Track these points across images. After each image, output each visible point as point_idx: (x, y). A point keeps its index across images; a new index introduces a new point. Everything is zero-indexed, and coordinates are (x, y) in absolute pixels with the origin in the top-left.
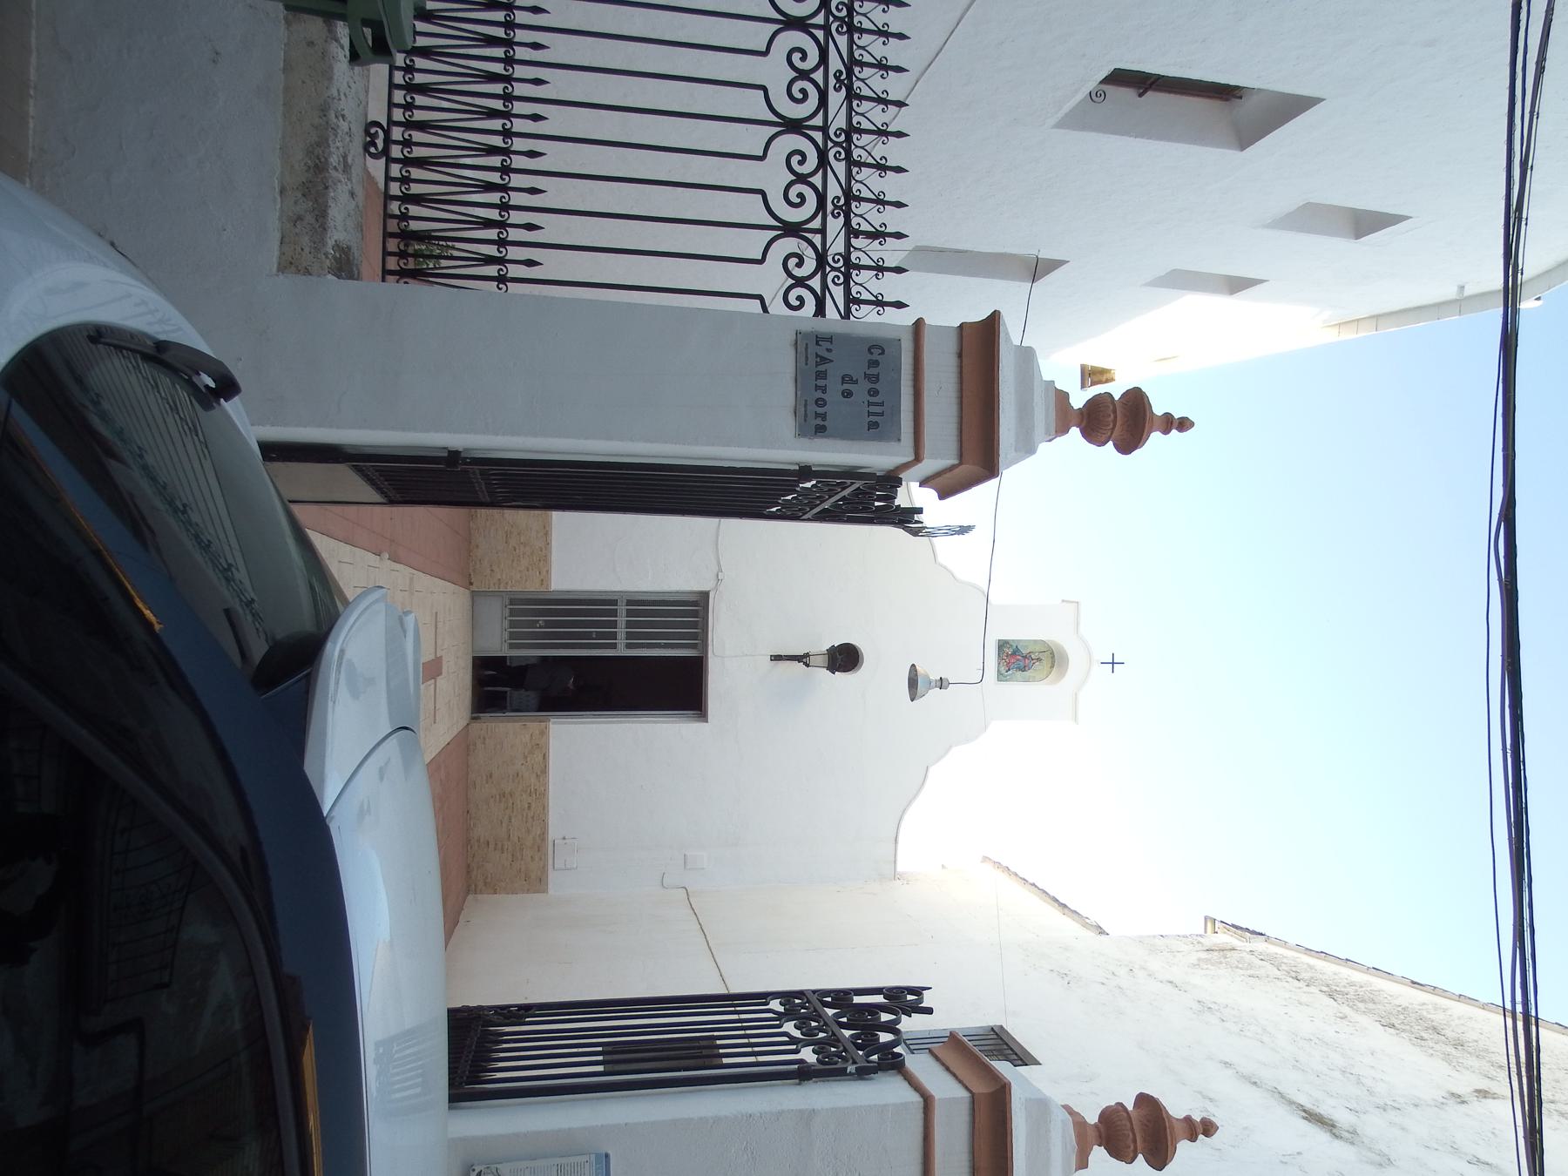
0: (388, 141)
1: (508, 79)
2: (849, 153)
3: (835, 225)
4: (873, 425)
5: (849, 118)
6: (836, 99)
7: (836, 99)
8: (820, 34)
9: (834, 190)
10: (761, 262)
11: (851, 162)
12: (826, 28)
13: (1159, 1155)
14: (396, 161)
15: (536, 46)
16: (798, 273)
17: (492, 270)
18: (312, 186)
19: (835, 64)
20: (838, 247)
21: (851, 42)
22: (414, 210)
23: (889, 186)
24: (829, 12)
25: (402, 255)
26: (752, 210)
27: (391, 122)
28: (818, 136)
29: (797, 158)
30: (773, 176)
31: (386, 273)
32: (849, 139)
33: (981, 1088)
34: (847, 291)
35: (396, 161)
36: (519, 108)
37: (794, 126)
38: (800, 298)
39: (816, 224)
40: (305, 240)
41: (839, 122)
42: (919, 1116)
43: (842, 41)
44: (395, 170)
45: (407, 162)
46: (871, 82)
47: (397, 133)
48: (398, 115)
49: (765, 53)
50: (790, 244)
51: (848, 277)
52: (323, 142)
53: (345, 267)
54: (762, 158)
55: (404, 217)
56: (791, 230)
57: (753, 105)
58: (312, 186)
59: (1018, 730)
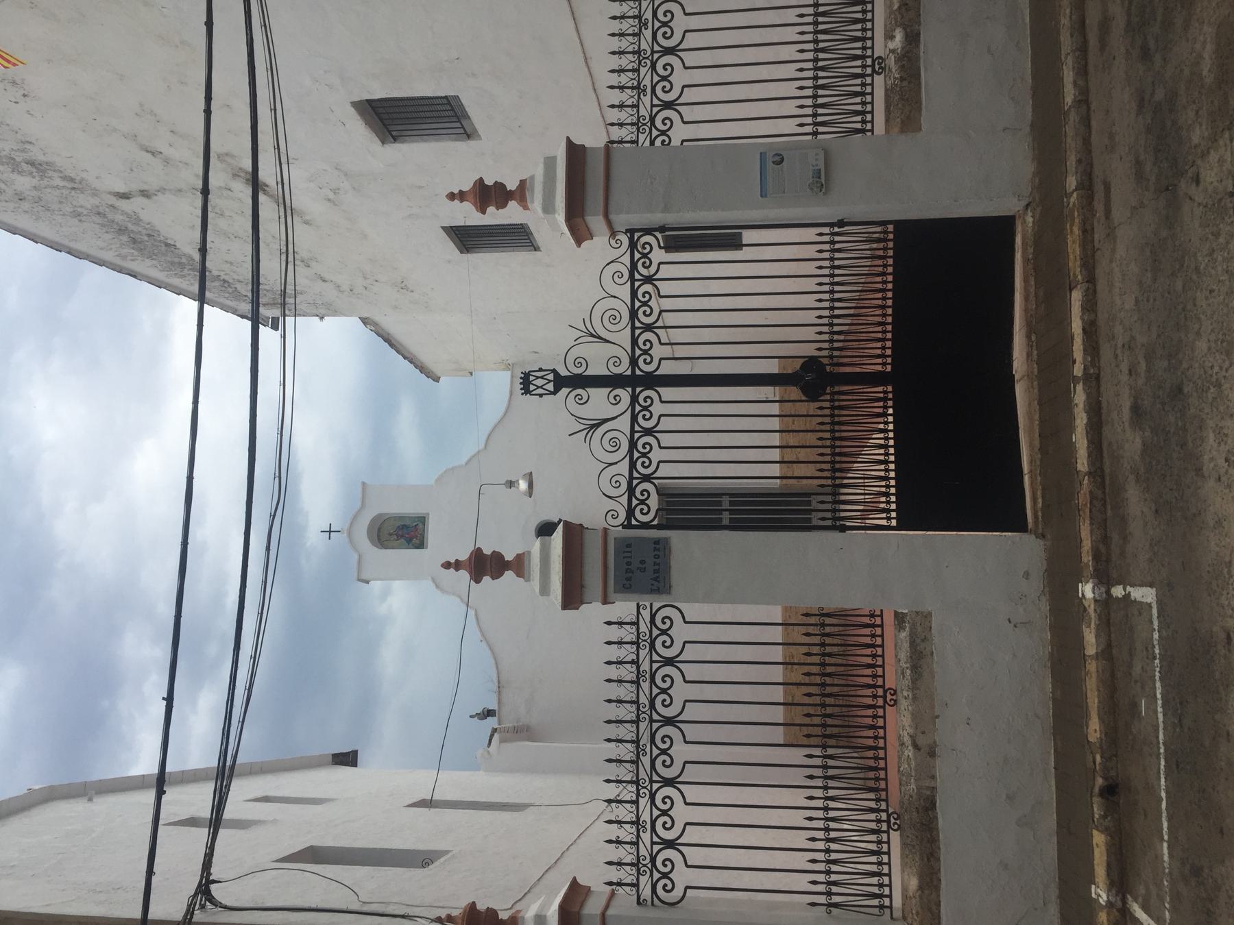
0: (888, 821)
1: (815, 124)
2: (638, 709)
3: (645, 666)
4: (629, 546)
5: (638, 808)
6: (645, 740)
7: (645, 740)
8: (655, 778)
9: (645, 686)
10: (685, 642)
11: (636, 702)
12: (651, 781)
13: (478, 554)
14: (883, 811)
15: (802, 107)
16: (666, 819)
17: (821, 9)
18: (919, 658)
19: (646, 760)
20: (643, 653)
21: (637, 776)
22: (873, 805)
23: (615, 653)
24: (650, 792)
25: (877, 779)
26: (692, 731)
27: (883, 707)
28: (655, 717)
29: (668, 644)
30: (680, 691)
31: (881, 616)
32: (638, 716)
33: (579, 220)
34: (638, 629)
35: (883, 811)
36: (821, 824)
37: (669, 721)
38: (665, 866)
39: (655, 666)
40: (919, 629)
41: (643, 726)
42: (611, 209)
43: (642, 774)
44: (869, 52)
45: (874, 686)
46: (626, 751)
47: (880, 702)
48: (869, 80)
49: (684, 87)
50: (668, 712)
51: (638, 637)
52: (914, 681)
53: (900, 618)
54: (687, 824)
55: (878, 800)
56: (669, 662)
57: (692, 671)
58: (919, 658)
59: (554, 347)
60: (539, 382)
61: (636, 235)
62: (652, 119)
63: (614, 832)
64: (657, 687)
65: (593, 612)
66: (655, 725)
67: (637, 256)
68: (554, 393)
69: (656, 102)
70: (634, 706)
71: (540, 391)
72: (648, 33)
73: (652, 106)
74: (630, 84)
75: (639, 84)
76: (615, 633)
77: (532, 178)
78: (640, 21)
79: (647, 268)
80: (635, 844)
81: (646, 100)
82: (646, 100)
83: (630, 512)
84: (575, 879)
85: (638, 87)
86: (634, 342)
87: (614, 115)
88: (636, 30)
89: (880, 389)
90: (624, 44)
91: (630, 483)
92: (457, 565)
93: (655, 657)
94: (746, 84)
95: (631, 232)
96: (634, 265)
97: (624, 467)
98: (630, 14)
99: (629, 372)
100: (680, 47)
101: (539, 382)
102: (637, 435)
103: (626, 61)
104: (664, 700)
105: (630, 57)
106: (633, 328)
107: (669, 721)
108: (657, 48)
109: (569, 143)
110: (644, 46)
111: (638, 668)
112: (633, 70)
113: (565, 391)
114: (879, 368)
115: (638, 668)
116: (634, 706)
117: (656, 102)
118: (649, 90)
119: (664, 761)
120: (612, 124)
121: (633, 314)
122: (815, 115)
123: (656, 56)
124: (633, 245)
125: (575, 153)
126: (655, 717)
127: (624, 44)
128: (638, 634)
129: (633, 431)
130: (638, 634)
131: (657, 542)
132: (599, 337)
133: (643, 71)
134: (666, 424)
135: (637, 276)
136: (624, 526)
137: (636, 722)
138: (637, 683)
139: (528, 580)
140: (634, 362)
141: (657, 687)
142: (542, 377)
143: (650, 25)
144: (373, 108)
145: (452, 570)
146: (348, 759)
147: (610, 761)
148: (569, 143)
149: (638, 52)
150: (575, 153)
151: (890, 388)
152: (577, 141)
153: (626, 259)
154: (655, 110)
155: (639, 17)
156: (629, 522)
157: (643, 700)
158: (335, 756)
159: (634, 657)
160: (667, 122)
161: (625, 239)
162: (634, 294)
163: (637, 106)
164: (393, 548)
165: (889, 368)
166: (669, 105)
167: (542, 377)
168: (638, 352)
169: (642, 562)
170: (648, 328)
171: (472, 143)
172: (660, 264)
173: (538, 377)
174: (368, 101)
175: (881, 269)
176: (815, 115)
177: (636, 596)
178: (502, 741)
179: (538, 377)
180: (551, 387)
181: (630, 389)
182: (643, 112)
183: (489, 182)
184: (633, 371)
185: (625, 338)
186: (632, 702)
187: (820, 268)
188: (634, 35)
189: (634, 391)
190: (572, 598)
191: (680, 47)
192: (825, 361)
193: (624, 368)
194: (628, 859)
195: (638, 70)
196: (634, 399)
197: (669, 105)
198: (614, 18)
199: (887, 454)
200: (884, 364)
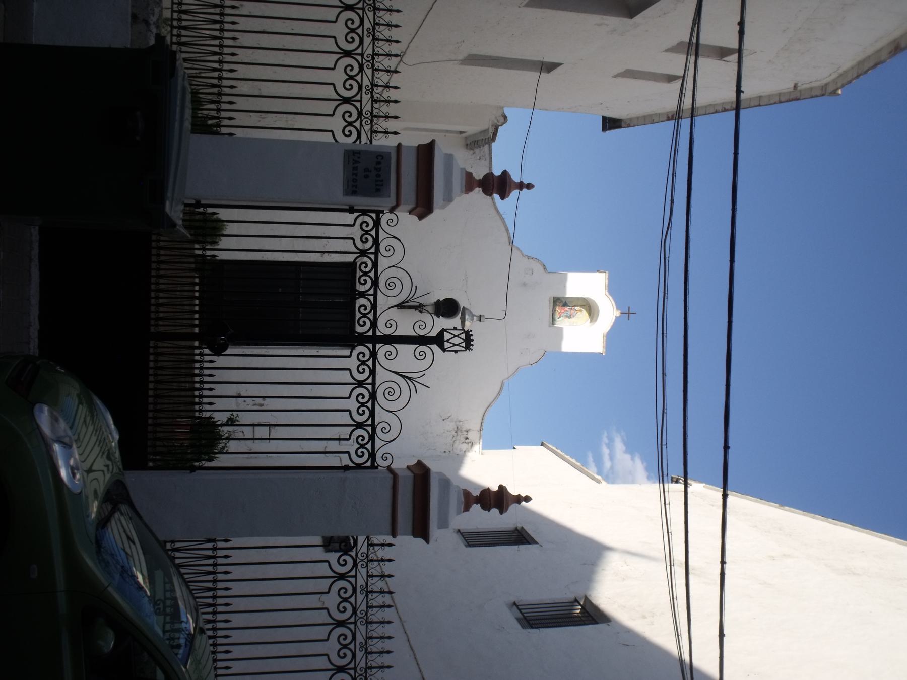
2: (373, 65)
3: (366, 98)
7: (367, 41)
8: (360, 12)
9: (366, 82)
11: (374, 70)
15: (227, 589)
19: (367, 25)
21: (375, 14)
23: (391, 110)
24: (356, 615)
29: (348, 114)
30: (338, 77)
32: (373, 59)
37: (348, 54)
39: (358, 98)
41: (370, 51)
43: (371, 14)
49: (328, 593)
50: (348, 61)
57: (329, 45)
60: (456, 341)
61: (369, 464)
62: (355, 564)
63: (394, 34)
64: (352, 556)
65: (412, 139)
66: (359, 51)
67: (369, 446)
68: (443, 330)
69: (352, 580)
70: (376, 67)
71: (456, 333)
72: (360, 639)
73: (355, 576)
74: (375, 595)
75: (367, 595)
76: (391, 125)
77: (458, 513)
78: (366, 649)
79: (365, 263)
80: (374, 132)
81: (361, 582)
82: (361, 582)
83: (377, 224)
84: (427, 541)
85: (368, 593)
86: (373, 372)
87: (388, 614)
88: (370, 641)
89: (162, 329)
90: (379, 630)
91: (377, 250)
92: (521, 186)
93: (358, 104)
94: (274, 580)
95: (373, 467)
96: (372, 438)
97: (383, 263)
98: (375, 656)
99: (378, 346)
100: (340, 9)
101: (456, 341)
102: (372, 292)
103: (377, 615)
104: (351, 70)
105: (375, 619)
106: (373, 384)
107: (348, 54)
108: (352, 626)
109: (426, 539)
110: (363, 628)
111: (372, 96)
112: (372, 607)
113: (434, 333)
114: (160, 344)
115: (372, 96)
116: (376, 67)
117: (352, 580)
118: (358, 590)
119: (353, 23)
120: (389, 606)
121: (373, 396)
122: (215, 581)
123: (352, 620)
124: (372, 455)
125: (421, 530)
126: (359, 58)
127: (379, 630)
128: (371, 123)
129: (375, 295)
130: (371, 123)
131: (354, 193)
132: (403, 377)
133: (364, 607)
134: (345, 391)
135: (369, 429)
136: (382, 212)
137: (374, 55)
138: (373, 85)
139: (463, 169)
140: (374, 354)
141: (352, 556)
142: (455, 345)
143: (358, 646)
144: (593, 619)
145: (526, 182)
146: (610, 124)
147: (397, 26)
148: (426, 539)
149: (368, 623)
150: (421, 530)
151: (152, 330)
152: (420, 541)
153: (378, 443)
154: (353, 573)
155: (367, 653)
156: (378, 216)
157: (369, 72)
158: (620, 127)
159: (375, 105)
160: (343, 563)
161: (379, 461)
162: (372, 414)
163: (368, 576)
164: (578, 299)
165: (152, 343)
166: (341, 577)
167: (455, 345)
168: (370, 363)
169: (366, 177)
170: (360, 384)
171: (512, 599)
172: (349, 439)
173: (458, 345)
174: (596, 623)
175: (159, 429)
176: (215, 581)
177: (372, 149)
178: (486, 131)
179: (458, 345)
180: (447, 336)
181: (378, 334)
182: (363, 571)
183: (495, 511)
184: (374, 347)
185: (381, 375)
186: (378, 70)
187: (211, 404)
188: (371, 638)
189: (374, 332)
190: (426, 152)
191: (340, 9)
192: (207, 351)
193: (382, 349)
194: (382, 13)
195: (368, 607)
196: (374, 325)
197: (341, 577)
198: (389, 652)
199: (156, 361)
200: (156, 347)
